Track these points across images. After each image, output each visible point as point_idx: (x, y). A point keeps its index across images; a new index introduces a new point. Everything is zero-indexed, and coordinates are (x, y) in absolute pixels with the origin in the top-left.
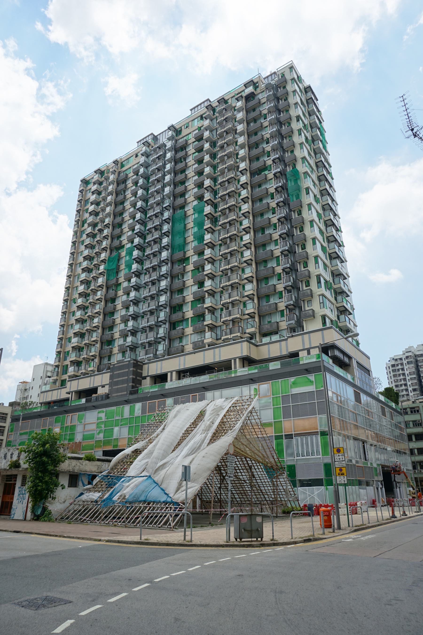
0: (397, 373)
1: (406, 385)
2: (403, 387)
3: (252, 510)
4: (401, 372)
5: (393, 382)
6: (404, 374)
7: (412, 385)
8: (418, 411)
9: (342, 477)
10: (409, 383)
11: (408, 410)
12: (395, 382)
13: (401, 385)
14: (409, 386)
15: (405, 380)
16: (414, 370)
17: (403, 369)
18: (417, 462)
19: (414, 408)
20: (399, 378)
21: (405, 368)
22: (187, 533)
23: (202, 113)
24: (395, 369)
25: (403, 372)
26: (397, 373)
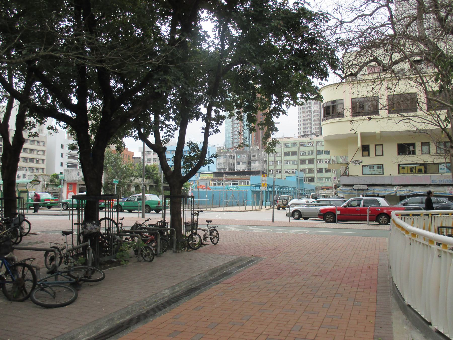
0: (306, 110)
1: (310, 119)
2: (309, 121)
3: (255, 188)
4: (309, 109)
5: (302, 117)
6: (310, 111)
7: (315, 125)
8: (312, 145)
9: (265, 187)
10: (313, 119)
11: (307, 143)
12: (303, 117)
13: (307, 120)
14: (312, 121)
15: (310, 116)
16: (318, 109)
17: (310, 107)
18: (307, 177)
19: (310, 142)
20: (306, 114)
21: (312, 106)
22: (166, 211)
23: (401, 163)
24: (305, 127)
25: (310, 110)
26: (306, 110)
